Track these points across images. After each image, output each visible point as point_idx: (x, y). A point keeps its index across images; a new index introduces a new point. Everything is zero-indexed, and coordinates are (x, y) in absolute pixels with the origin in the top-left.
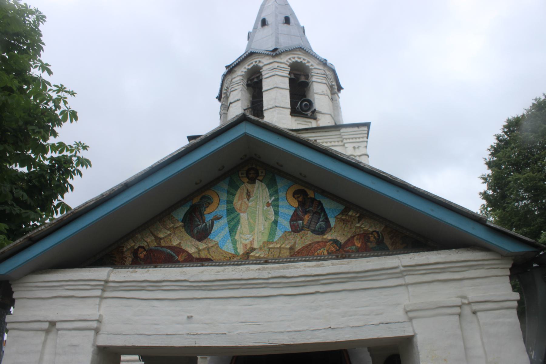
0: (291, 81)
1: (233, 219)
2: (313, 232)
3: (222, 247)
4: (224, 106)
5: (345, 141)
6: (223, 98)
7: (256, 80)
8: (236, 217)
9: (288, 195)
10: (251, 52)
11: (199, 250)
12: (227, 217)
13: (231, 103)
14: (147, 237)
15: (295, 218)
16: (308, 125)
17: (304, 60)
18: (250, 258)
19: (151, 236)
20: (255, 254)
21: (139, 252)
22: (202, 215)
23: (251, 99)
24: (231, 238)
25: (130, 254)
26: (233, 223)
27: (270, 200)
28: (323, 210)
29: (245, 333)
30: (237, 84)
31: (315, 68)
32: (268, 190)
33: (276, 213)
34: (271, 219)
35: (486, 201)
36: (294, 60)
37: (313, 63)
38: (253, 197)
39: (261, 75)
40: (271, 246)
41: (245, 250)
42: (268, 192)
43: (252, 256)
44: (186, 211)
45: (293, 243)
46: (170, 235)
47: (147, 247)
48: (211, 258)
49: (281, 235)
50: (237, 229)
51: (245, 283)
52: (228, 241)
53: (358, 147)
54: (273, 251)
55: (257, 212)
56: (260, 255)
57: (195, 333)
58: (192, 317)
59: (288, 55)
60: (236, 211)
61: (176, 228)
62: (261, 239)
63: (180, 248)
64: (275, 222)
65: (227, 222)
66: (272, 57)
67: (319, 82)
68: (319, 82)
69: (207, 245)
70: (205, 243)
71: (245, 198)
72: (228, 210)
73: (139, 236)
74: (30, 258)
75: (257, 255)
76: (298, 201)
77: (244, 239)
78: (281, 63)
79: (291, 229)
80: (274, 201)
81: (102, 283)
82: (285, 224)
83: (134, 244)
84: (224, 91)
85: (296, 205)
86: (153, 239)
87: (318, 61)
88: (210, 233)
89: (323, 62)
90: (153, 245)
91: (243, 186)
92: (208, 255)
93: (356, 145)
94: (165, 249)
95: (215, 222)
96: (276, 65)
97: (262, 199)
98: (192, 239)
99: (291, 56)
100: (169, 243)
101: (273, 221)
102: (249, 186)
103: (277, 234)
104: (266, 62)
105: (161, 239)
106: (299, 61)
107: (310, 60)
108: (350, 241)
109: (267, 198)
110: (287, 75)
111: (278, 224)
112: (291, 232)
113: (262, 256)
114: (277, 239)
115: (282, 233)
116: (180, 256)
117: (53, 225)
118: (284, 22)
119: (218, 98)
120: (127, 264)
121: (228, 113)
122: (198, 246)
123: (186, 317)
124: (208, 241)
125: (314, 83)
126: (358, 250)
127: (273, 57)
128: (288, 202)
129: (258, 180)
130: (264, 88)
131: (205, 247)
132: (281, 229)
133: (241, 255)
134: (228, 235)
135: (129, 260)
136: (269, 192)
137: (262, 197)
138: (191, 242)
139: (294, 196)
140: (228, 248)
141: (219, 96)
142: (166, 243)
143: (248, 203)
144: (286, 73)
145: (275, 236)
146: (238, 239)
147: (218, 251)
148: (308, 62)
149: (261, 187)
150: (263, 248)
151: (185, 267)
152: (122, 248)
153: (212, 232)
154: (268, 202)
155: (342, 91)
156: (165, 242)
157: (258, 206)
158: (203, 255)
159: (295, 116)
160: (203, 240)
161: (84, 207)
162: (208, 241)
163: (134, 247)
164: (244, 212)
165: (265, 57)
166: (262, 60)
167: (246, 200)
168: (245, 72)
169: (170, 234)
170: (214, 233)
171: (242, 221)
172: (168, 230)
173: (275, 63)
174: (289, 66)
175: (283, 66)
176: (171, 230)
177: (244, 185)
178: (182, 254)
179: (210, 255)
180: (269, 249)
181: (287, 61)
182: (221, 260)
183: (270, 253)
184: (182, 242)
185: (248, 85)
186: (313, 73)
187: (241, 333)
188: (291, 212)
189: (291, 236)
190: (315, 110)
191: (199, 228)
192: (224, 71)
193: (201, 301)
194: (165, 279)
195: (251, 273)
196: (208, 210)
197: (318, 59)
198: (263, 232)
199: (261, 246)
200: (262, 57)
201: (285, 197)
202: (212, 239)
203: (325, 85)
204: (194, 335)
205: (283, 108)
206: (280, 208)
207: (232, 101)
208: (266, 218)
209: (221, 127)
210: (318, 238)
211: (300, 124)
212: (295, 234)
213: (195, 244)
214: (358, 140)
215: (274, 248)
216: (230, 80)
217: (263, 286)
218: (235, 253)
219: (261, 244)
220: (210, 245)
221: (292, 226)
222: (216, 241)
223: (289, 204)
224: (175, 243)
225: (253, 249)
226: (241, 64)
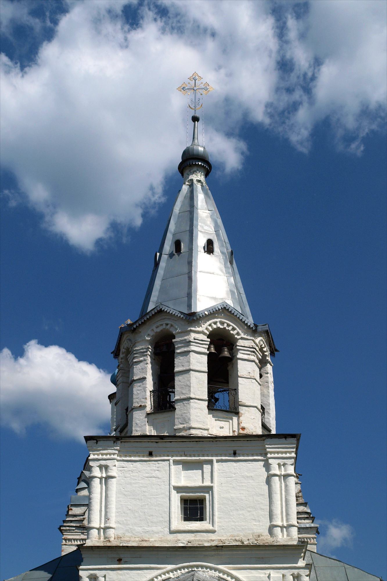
4: (123, 371)
5: (269, 455)
6: (122, 359)
31: (242, 338)
35: (99, 242)
36: (215, 326)
53: (284, 465)
93: (281, 461)
107: (240, 332)
148: (234, 329)
181: (207, 329)
186: (239, 346)
214: (284, 455)
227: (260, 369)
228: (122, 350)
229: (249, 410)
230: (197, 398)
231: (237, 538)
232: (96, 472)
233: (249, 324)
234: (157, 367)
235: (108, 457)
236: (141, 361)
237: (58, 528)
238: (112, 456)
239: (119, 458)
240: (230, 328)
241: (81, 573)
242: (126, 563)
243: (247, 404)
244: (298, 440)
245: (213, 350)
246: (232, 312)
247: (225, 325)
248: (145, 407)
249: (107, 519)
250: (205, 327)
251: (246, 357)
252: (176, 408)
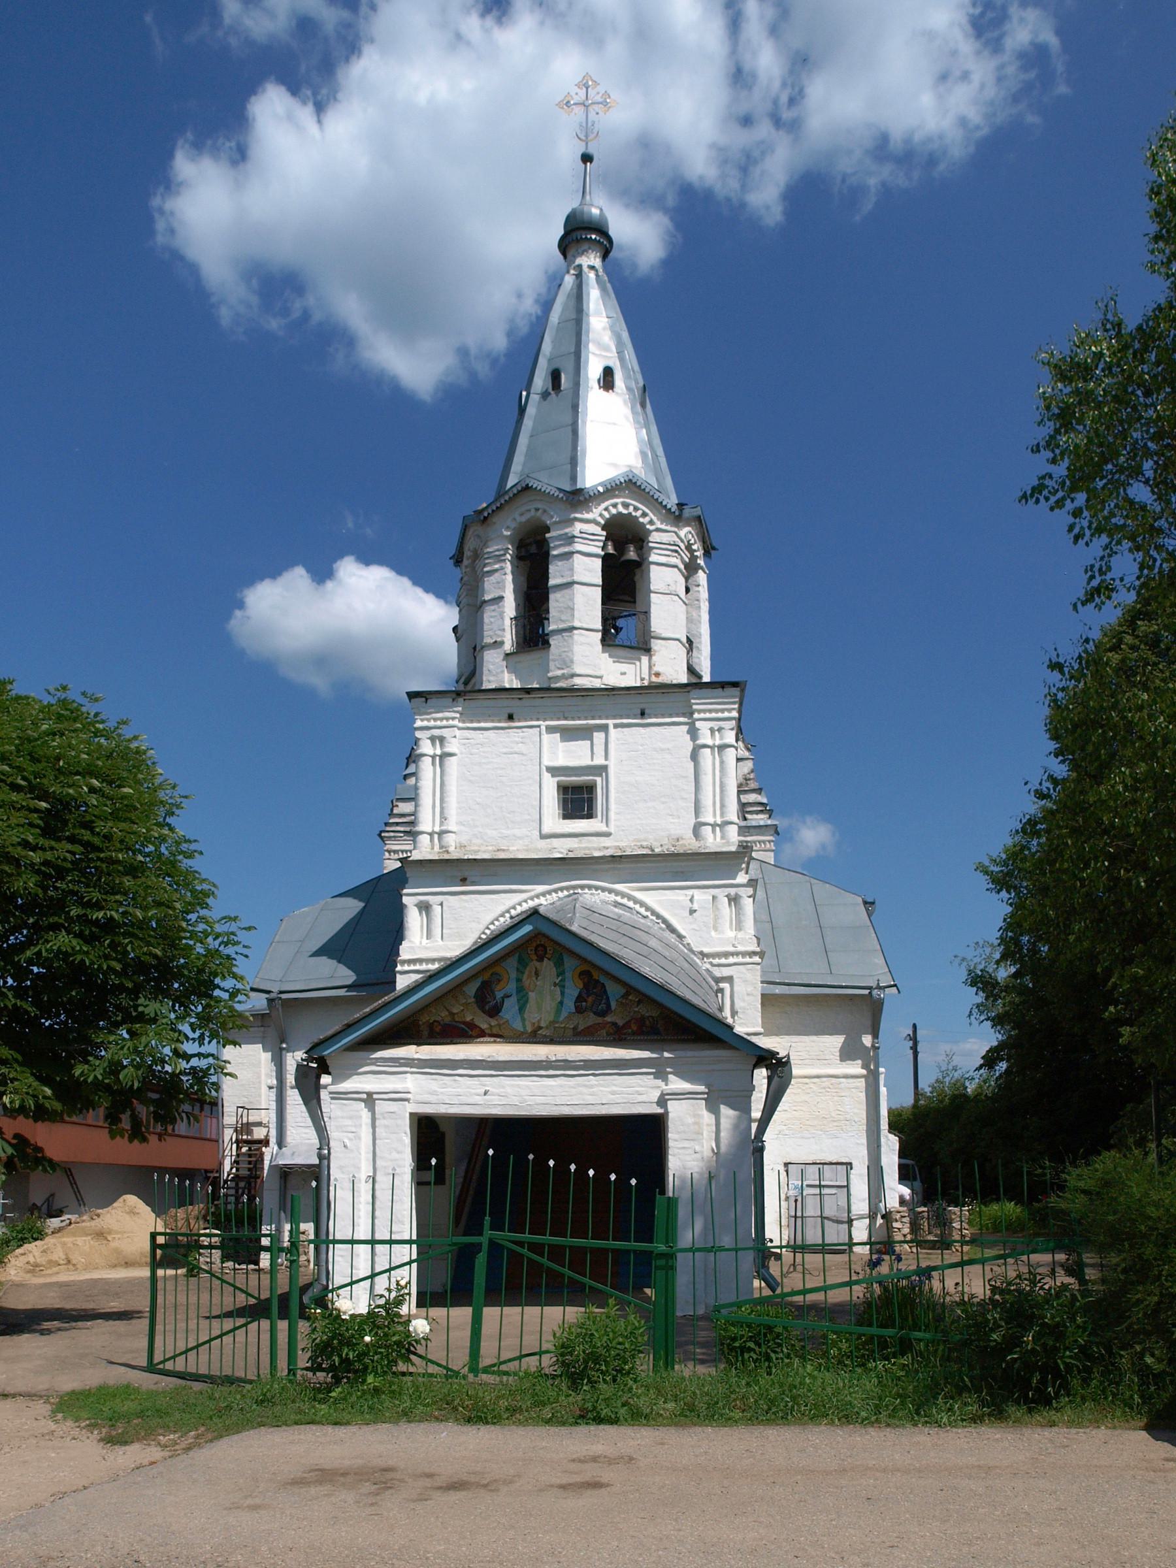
1: (524, 996)
2: (595, 1013)
5: (696, 716)
6: (466, 567)
11: (491, 1026)
15: (579, 999)
22: (493, 992)
23: (525, 589)
28: (605, 992)
31: (658, 530)
33: (562, 993)
36: (614, 511)
53: (720, 730)
64: (561, 1003)
80: (561, 981)
82: (570, 1005)
85: (581, 986)
90: (448, 1020)
94: (458, 1024)
102: (538, 964)
105: (454, 1014)
108: (627, 1025)
126: (634, 1034)
140: (518, 1025)
148: (644, 515)
171: (530, 1000)
174: (603, 530)
180: (555, 1028)
181: (601, 515)
188: (576, 994)
196: (498, 987)
203: (676, 570)
210: (600, 1020)
214: (720, 715)
215: (559, 1027)
224: (468, 1019)
225: (540, 1028)
226: (506, 508)
227: (687, 579)
228: (467, 553)
231: (645, 844)
232: (426, 747)
234: (522, 579)
235: (445, 723)
236: (496, 571)
238: (451, 722)
239: (461, 725)
240: (639, 513)
241: (405, 900)
242: (474, 883)
243: (664, 635)
244: (743, 691)
245: (610, 550)
247: (631, 508)
248: (502, 643)
249: (443, 818)
250: (599, 512)
251: (663, 560)
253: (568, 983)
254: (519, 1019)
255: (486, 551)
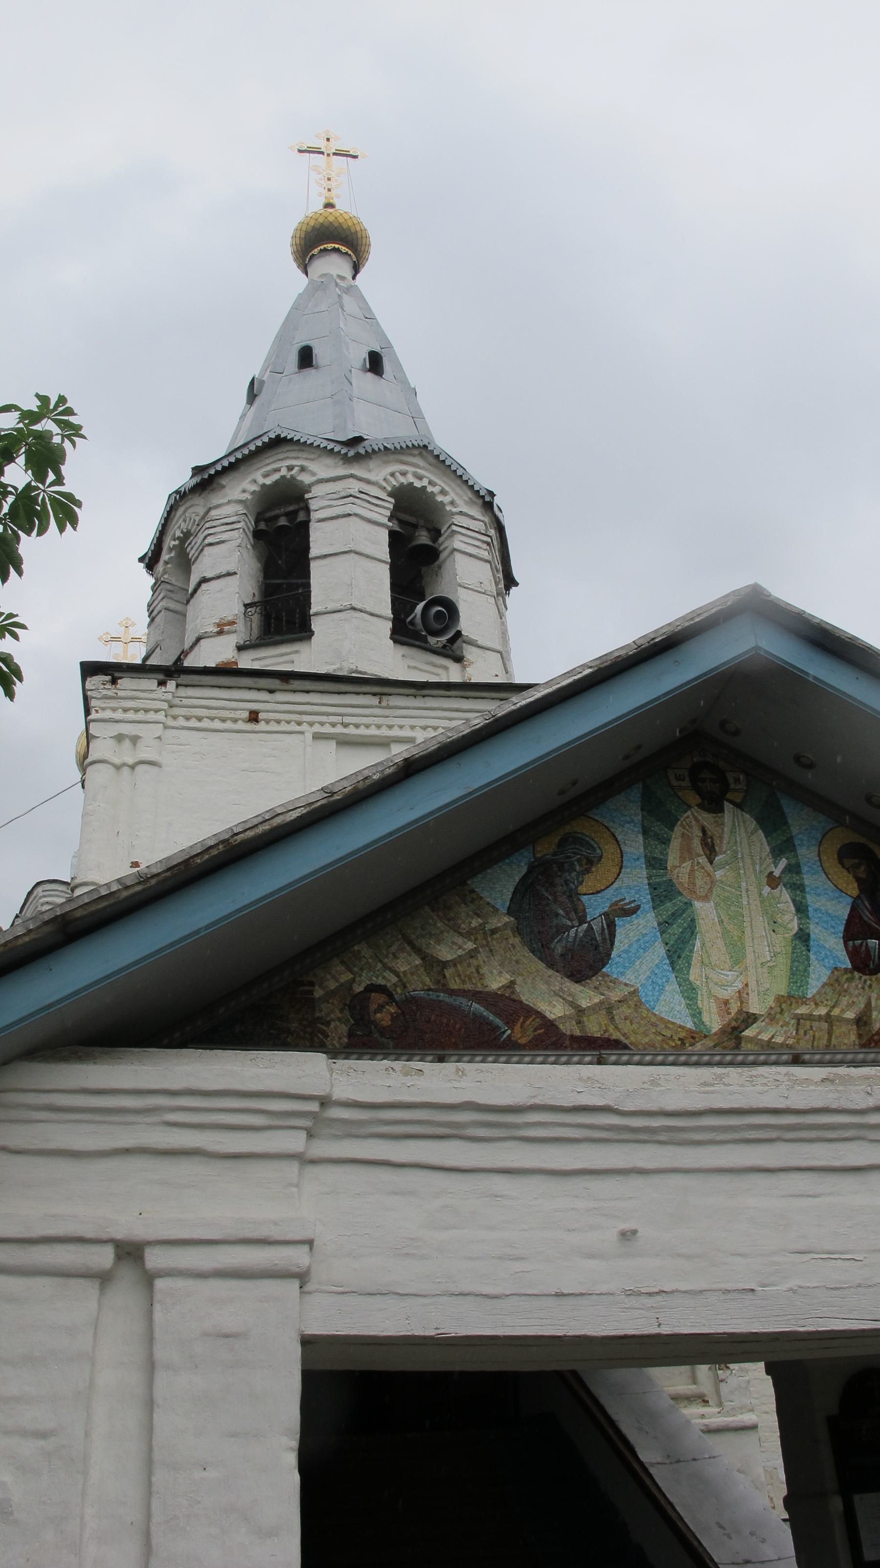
0: (395, 539)
1: (675, 916)
3: (652, 1003)
4: (169, 587)
6: (166, 563)
7: (283, 522)
8: (684, 911)
9: (824, 858)
10: (278, 436)
11: (580, 1011)
12: (654, 908)
13: (205, 580)
14: (395, 957)
16: (438, 675)
17: (431, 483)
18: (743, 1044)
19: (410, 955)
20: (759, 1033)
21: (373, 1007)
23: (261, 579)
24: (676, 977)
25: (341, 1011)
26: (676, 929)
27: (776, 867)
29: (814, 1287)
30: (227, 524)
32: (766, 837)
33: (801, 909)
34: (789, 926)
36: (402, 480)
37: (456, 498)
38: (724, 853)
39: (308, 510)
40: (802, 1010)
41: (727, 1019)
42: (766, 843)
43: (751, 1040)
44: (517, 879)
45: (862, 1006)
46: (472, 954)
47: (399, 990)
48: (622, 1039)
49: (824, 979)
50: (691, 951)
51: (799, 1124)
52: (667, 988)
54: (808, 1027)
55: (745, 903)
56: (773, 1037)
57: (656, 1290)
58: (634, 1232)
59: (387, 463)
60: (680, 894)
61: (493, 932)
62: (767, 986)
63: (514, 1001)
64: (803, 937)
65: (656, 924)
66: (341, 462)
67: (471, 555)
68: (471, 555)
69: (603, 994)
70: (596, 988)
71: (699, 855)
72: (653, 887)
73: (365, 950)
74: (56, 997)
75: (765, 1037)
76: (858, 880)
77: (716, 984)
78: (368, 482)
79: (851, 962)
80: (789, 869)
81: (314, 1107)
83: (351, 976)
84: (169, 542)
86: (417, 963)
87: (470, 494)
88: (609, 956)
89: (483, 497)
91: (688, 817)
92: (611, 1029)
94: (463, 1002)
95: (618, 922)
96: (354, 486)
97: (749, 861)
98: (551, 972)
99: (396, 467)
100: (474, 981)
101: (794, 932)
102: (706, 818)
103: (812, 976)
104: (323, 474)
105: (444, 965)
106: (418, 484)
107: (447, 488)
109: (765, 859)
110: (385, 520)
111: (812, 943)
112: (851, 972)
113: (779, 1040)
114: (815, 991)
115: (828, 973)
116: (517, 1027)
117: (153, 882)
118: (368, 366)
119: (147, 560)
120: (333, 1045)
121: (191, 610)
122: (570, 995)
123: (612, 1235)
124: (606, 982)
125: (458, 556)
127: (347, 460)
128: (828, 877)
129: (731, 802)
130: (314, 552)
131: (596, 1000)
132: (823, 960)
133: (715, 1034)
134: (666, 967)
135: (339, 1030)
136: (769, 844)
137: (752, 857)
138: (548, 983)
139: (841, 861)
141: (150, 555)
142: (464, 982)
143: (712, 869)
144: (382, 514)
145: (808, 979)
146: (698, 983)
147: (643, 1018)
148: (443, 492)
149: (741, 824)
150: (778, 1016)
151: (579, 1063)
152: (306, 988)
153: (614, 954)
154: (772, 873)
155: (514, 590)
156: (459, 976)
157: (744, 884)
158: (594, 1027)
159: (402, 643)
160: (589, 977)
161: (266, 827)
162: (606, 982)
163: (350, 988)
164: (706, 898)
165: (319, 457)
166: (312, 466)
167: (703, 860)
168: (254, 493)
169: (476, 950)
170: (619, 956)
171: (702, 925)
172: (469, 934)
173: (351, 480)
175: (375, 491)
176: (476, 939)
177: (689, 813)
178: (524, 1022)
179: (616, 1028)
180: (799, 1018)
182: (653, 1046)
183: (801, 1032)
184: (519, 980)
185: (257, 535)
187: (800, 1287)
188: (843, 911)
189: (853, 984)
190: (459, 634)
191: (571, 940)
192: (183, 478)
193: (656, 1179)
194: (537, 1101)
195: (814, 1090)
196: (589, 883)
197: (472, 487)
198: (769, 964)
199: (771, 1008)
200: (312, 456)
201: (819, 864)
202: (615, 976)
203: (488, 565)
204: (650, 1294)
205: (372, 614)
206: (810, 893)
207: (209, 575)
208: (775, 922)
209: (692, 619)
211: (415, 668)
212: (864, 977)
213: (561, 989)
215: (810, 1017)
216: (201, 511)
217: (848, 1134)
218: (696, 1028)
219: (771, 1001)
220: (615, 996)
221: (853, 954)
222: (632, 986)
223: (832, 885)
224: (495, 982)
225: (750, 1019)
226: (242, 468)
229: (484, 655)
230: (367, 610)
233: (476, 488)
234: (259, 565)
235: (140, 716)
237: (60, 395)
238: (151, 716)
243: (480, 643)
246: (441, 458)
252: (314, 632)
253: (812, 879)
254: (672, 987)
255: (190, 556)
